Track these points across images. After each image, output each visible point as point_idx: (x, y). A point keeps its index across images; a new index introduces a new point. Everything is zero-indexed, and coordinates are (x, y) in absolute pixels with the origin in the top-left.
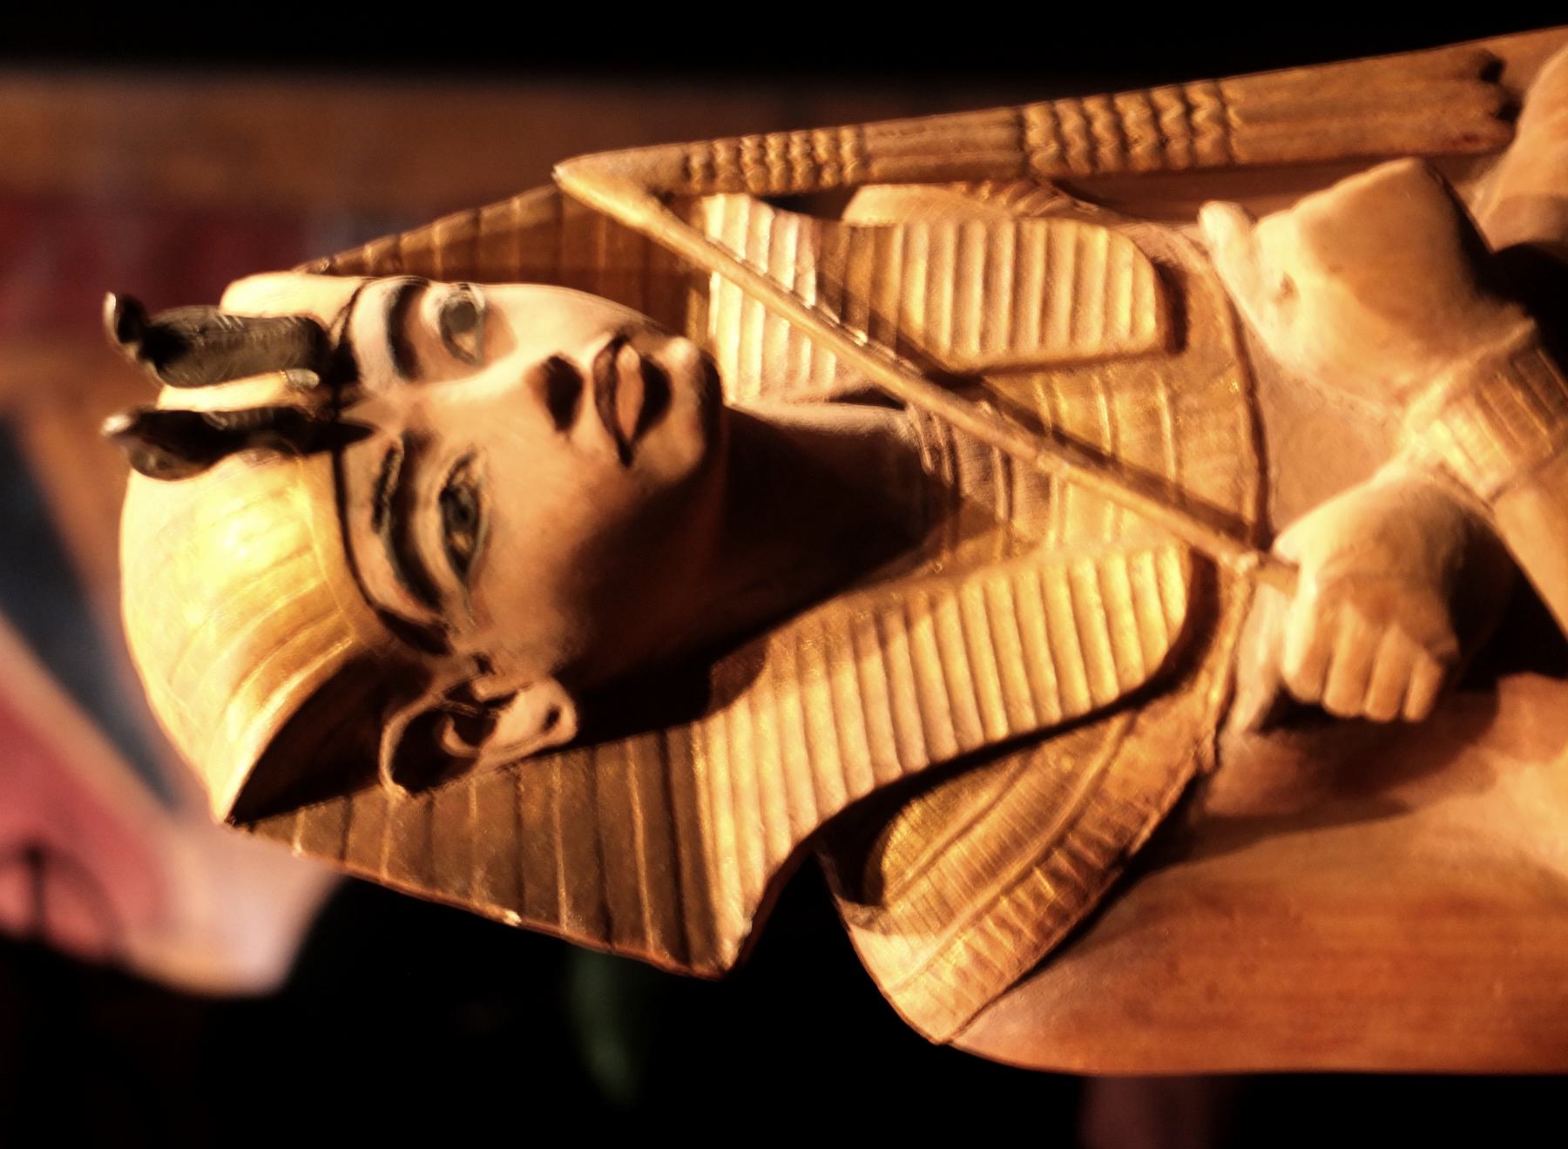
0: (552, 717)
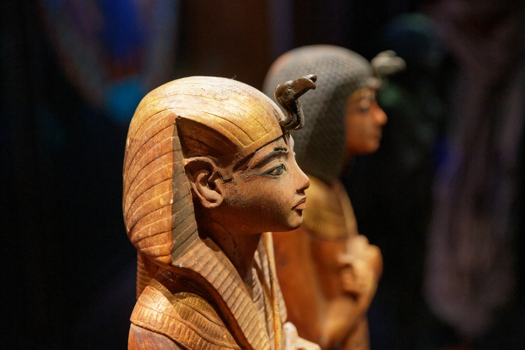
0: (213, 201)
